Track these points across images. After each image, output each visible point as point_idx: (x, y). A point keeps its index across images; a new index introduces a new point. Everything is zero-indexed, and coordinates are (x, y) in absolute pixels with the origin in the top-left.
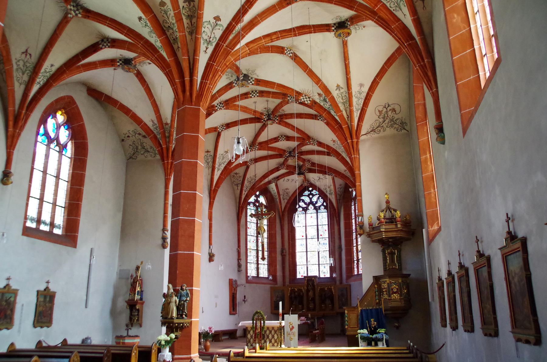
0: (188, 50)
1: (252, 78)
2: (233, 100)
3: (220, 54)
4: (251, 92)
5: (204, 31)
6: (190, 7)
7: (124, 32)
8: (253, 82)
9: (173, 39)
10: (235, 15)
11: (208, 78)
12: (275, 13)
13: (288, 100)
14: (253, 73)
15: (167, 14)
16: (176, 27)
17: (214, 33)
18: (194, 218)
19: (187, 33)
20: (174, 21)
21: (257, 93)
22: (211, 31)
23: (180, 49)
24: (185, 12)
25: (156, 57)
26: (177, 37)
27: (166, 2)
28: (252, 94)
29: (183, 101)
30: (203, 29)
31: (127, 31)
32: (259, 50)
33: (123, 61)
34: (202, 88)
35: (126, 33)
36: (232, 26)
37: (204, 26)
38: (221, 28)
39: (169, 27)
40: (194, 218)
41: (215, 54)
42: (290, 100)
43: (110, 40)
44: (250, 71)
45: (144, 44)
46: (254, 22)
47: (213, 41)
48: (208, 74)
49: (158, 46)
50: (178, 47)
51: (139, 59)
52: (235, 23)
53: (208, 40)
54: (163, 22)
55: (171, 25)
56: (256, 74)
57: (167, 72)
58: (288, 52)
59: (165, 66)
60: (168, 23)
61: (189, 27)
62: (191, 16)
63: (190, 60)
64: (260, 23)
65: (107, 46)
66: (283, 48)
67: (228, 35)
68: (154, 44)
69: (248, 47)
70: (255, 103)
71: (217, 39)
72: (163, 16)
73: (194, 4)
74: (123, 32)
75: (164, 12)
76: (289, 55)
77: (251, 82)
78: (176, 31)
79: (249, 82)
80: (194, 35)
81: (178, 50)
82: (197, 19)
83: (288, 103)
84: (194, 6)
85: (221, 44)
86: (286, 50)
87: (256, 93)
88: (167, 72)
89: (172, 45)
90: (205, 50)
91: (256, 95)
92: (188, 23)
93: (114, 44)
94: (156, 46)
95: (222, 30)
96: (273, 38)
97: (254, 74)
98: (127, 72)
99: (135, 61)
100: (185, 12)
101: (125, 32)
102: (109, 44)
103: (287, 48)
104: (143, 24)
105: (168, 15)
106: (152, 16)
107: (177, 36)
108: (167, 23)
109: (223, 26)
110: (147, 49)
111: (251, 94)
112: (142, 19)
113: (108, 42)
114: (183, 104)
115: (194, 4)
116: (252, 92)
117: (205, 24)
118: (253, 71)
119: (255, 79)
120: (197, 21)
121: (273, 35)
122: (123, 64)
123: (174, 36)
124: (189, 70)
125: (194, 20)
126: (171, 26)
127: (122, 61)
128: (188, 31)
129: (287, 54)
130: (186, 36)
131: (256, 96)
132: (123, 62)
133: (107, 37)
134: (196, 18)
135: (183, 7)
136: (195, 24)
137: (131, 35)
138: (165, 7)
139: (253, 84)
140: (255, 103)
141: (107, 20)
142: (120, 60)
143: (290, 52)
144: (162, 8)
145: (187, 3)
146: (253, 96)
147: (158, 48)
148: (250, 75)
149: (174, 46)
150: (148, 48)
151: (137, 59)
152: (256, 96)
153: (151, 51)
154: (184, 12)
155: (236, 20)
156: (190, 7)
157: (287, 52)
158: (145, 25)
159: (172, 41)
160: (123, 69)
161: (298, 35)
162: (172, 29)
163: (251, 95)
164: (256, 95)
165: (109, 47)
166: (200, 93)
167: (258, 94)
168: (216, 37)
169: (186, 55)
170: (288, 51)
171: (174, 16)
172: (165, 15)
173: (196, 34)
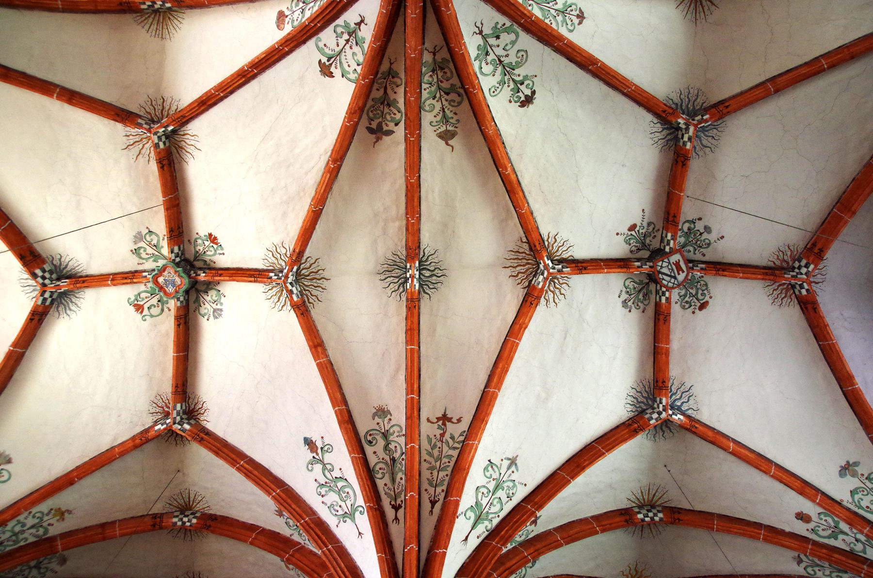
6: (380, 120)
9: (446, 70)
15: (444, 116)
18: (15, 349)
39: (447, 94)
40: (15, 349)
61: (395, 87)
62: (382, 103)
72: (455, 114)
73: (370, 124)
75: (451, 120)
78: (431, 84)
84: (371, 120)
100: (395, 114)
105: (441, 115)
107: (431, 76)
108: (450, 102)
112: (523, 98)
117: (353, 76)
125: (377, 94)
126: (442, 93)
135: (396, 125)
136: (376, 86)
138: (443, 129)
144: (450, 128)
145: (385, 128)
159: (451, 65)
162: (439, 88)
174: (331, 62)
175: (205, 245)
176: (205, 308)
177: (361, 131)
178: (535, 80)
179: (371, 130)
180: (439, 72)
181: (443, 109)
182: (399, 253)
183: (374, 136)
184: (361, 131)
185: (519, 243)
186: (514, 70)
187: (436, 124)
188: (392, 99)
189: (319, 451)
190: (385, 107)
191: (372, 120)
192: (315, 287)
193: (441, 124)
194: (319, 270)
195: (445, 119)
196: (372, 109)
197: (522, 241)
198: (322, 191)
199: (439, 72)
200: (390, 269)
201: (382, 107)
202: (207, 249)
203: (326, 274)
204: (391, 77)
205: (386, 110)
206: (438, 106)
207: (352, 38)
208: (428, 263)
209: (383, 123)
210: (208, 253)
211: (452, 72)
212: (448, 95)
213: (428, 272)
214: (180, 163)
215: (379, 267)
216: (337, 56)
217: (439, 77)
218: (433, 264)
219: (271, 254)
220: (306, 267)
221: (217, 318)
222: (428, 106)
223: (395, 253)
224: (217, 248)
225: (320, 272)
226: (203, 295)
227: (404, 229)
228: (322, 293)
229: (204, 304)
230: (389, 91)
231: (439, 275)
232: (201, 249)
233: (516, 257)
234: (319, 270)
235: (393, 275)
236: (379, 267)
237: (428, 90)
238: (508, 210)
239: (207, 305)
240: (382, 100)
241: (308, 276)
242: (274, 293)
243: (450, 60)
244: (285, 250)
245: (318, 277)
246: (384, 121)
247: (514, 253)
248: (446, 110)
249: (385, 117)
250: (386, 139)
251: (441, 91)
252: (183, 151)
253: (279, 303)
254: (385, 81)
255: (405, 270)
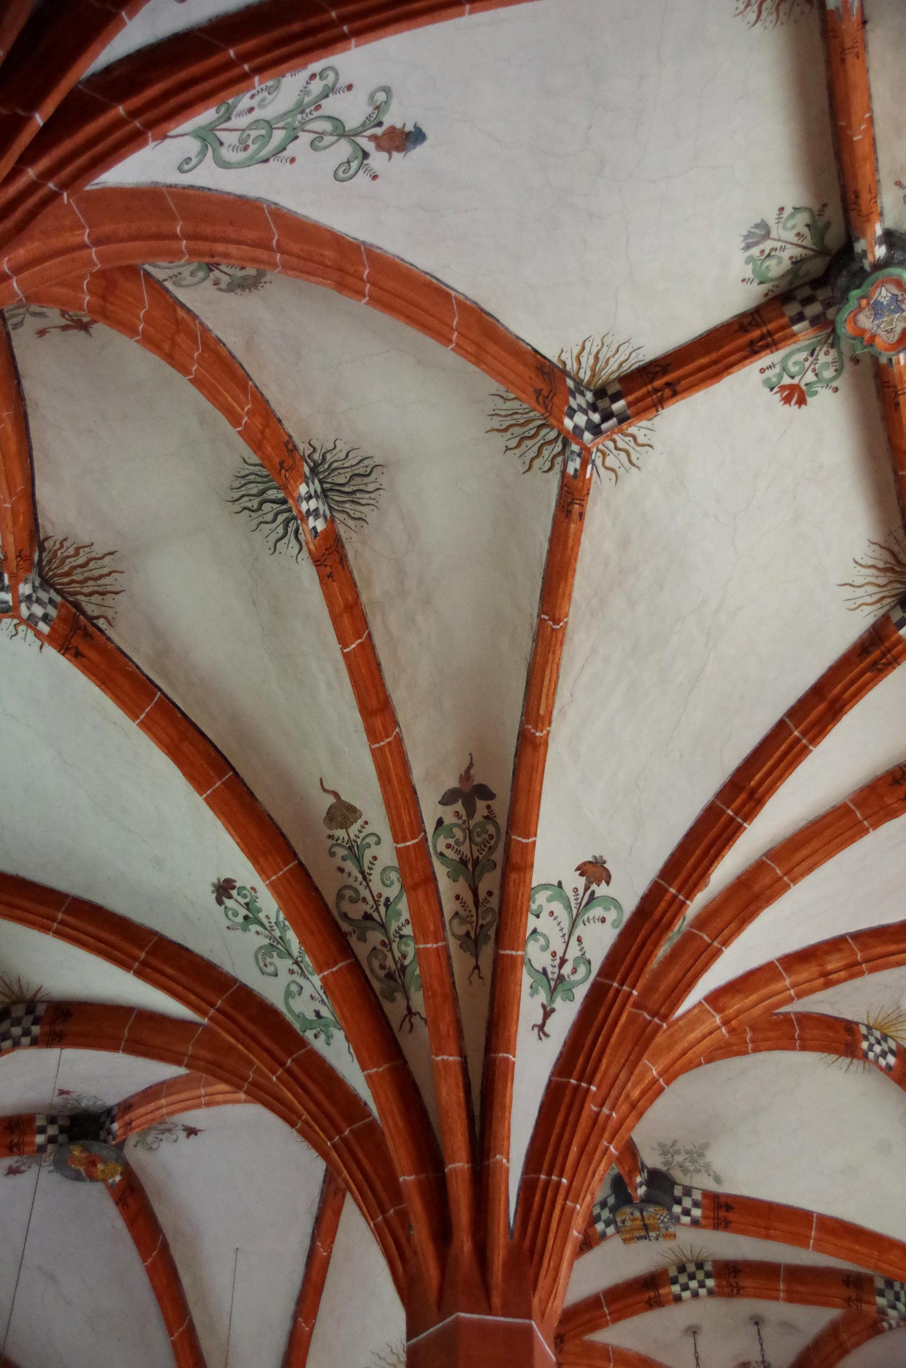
0: (458, 1024)
1: (688, 1191)
2: (587, 1317)
3: (613, 1040)
4: (673, 1272)
5: (535, 931)
6: (472, 823)
7: (135, 958)
8: (697, 1213)
9: (382, 973)
10: (673, 855)
11: (560, 1158)
12: (852, 840)
13: (882, 1312)
14: (693, 1161)
15: (358, 860)
16: (406, 915)
17: (579, 940)
19: (453, 945)
20: (393, 892)
21: (708, 1275)
22: (566, 931)
23: (416, 1020)
24: (448, 846)
25: (289, 1071)
26: (406, 962)
27: (357, 805)
28: (683, 1279)
29: (441, 1289)
30: (532, 922)
31: (151, 953)
32: (749, 1035)
33: (65, 1123)
34: (534, 1214)
35: (144, 963)
36: (663, 904)
37: (534, 907)
38: (611, 915)
39: (367, 917)
41: (590, 1037)
42: (892, 1313)
43: (41, 1009)
44: (678, 1152)
45: (228, 1009)
46: (756, 888)
47: (573, 978)
48: (561, 1136)
49: (300, 1016)
50: (410, 1012)
51: (152, 1106)
52: (679, 891)
53: (552, 973)
54: (340, 896)
55: (377, 910)
56: (707, 1168)
57: (344, 1140)
58: (878, 1049)
59: (332, 1111)
60: (364, 899)
61: (462, 912)
62: (476, 862)
63: (470, 1069)
64: (786, 887)
65: (26, 1040)
66: (850, 1027)
67: (648, 946)
68: (280, 1006)
69: (720, 1010)
70: (693, 1331)
71: (596, 967)
72: (341, 870)
73: (488, 807)
74: (128, 955)
75: (345, 852)
76: (882, 1062)
77: (686, 1212)
78: (401, 937)
79: (677, 1209)
80: (487, 951)
81: (406, 1025)
82: (504, 876)
83: (875, 1328)
84: (489, 818)
85: (618, 991)
86: (866, 1038)
87: (700, 1275)
88: (344, 1140)
89: (379, 1004)
90: (540, 1022)
91: (702, 1285)
92: (457, 897)
93: (58, 1028)
94: (289, 1017)
95: (614, 925)
96: (830, 967)
97: (698, 1171)
98: (78, 1178)
99: (127, 1118)
100: (448, 846)
101: (143, 955)
102: (36, 1030)
103: (869, 1028)
104: (236, 914)
105: (366, 864)
106: (290, 870)
107: (404, 956)
109: (619, 907)
110: (243, 1030)
111: (674, 1281)
112: (234, 893)
113: (30, 1018)
114: (443, 1307)
115: (488, 807)
116: (682, 1269)
117: (540, 898)
118: (697, 1154)
119: (706, 1194)
120: (503, 886)
121: (827, 953)
122: (62, 1138)
123: (390, 962)
124: (466, 1122)
125: (489, 882)
126: (375, 915)
127: (61, 1122)
128: (461, 930)
129: (871, 1055)
130: (449, 957)
131: (703, 1292)
132: (62, 1130)
133: (29, 995)
134: (499, 870)
135: (440, 822)
136: (494, 902)
137: (170, 971)
138: (354, 829)
139: (695, 1223)
140: (693, 1331)
141: (59, 909)
142: (52, 1120)
143: (885, 1046)
144: (340, 833)
145: (459, 806)
146: (686, 1295)
147: (297, 1026)
148: (677, 1174)
149: (386, 1005)
150: (251, 1027)
151: (142, 1110)
152: (703, 1292)
153: (267, 1042)
154: (441, 847)
155: (684, 873)
156: (472, 823)
157: (871, 1047)
158: (246, 918)
159: (376, 985)
160: (61, 1165)
161: (668, 1083)
162: (383, 926)
163: (676, 1289)
164: (702, 1285)
165: (35, 1043)
166: (527, 1243)
167: (710, 1283)
168: (588, 956)
169: (452, 1045)
170: (872, 1040)
171: (401, 870)
172: (350, 866)
173: (499, 942)
174: (589, 892)
175: (814, 370)
176: (794, 227)
177: (501, 786)
178: (228, 923)
179: (484, 792)
180: (393, 967)
181: (365, 878)
182: (351, 523)
183: (475, 783)
184: (501, 786)
185: (110, 614)
186: (271, 945)
187: (367, 840)
188: (461, 879)
189: (369, 146)
190: (469, 856)
191: (486, 818)
192: (517, 413)
193: (359, 841)
194: (519, 445)
195: (355, 852)
196: (492, 842)
197: (106, 618)
198: (548, 672)
199: (393, 967)
200: (358, 480)
201: (476, 854)
202: (807, 364)
203: (500, 440)
204: (473, 935)
205: (465, 848)
206: (376, 885)
207: (555, 976)
208: (281, 518)
209: (465, 818)
210: (804, 355)
211: (372, 970)
212: (366, 913)
213: (273, 497)
214: (890, 533)
215: (384, 480)
216: (577, 916)
217: (389, 954)
218: (270, 517)
219: (641, 440)
220: (550, 448)
221: (757, 226)
222: (392, 883)
223: (360, 522)
224: (780, 377)
225: (514, 443)
226: (806, 251)
227: (359, 583)
228: (495, 407)
229: (798, 234)
230: (468, 897)
231: (246, 498)
232: (822, 359)
233: (99, 582)
234: (519, 445)
235: (349, 470)
236: (384, 480)
237: (403, 920)
238: (165, 675)
239: (790, 236)
240: (478, 868)
241: (540, 427)
242: (611, 361)
243: (381, 999)
244: (607, 464)
245: (518, 430)
246: (464, 822)
247: (109, 588)
248: (360, 877)
249: (464, 831)
250: (453, 783)
251: (380, 921)
252: (881, 565)
253: (594, 351)
254: (481, 922)
255: (325, 486)
